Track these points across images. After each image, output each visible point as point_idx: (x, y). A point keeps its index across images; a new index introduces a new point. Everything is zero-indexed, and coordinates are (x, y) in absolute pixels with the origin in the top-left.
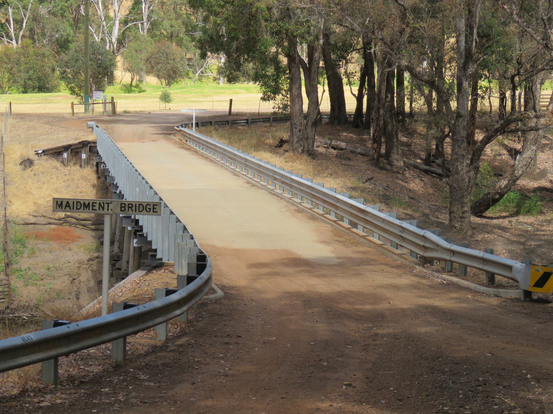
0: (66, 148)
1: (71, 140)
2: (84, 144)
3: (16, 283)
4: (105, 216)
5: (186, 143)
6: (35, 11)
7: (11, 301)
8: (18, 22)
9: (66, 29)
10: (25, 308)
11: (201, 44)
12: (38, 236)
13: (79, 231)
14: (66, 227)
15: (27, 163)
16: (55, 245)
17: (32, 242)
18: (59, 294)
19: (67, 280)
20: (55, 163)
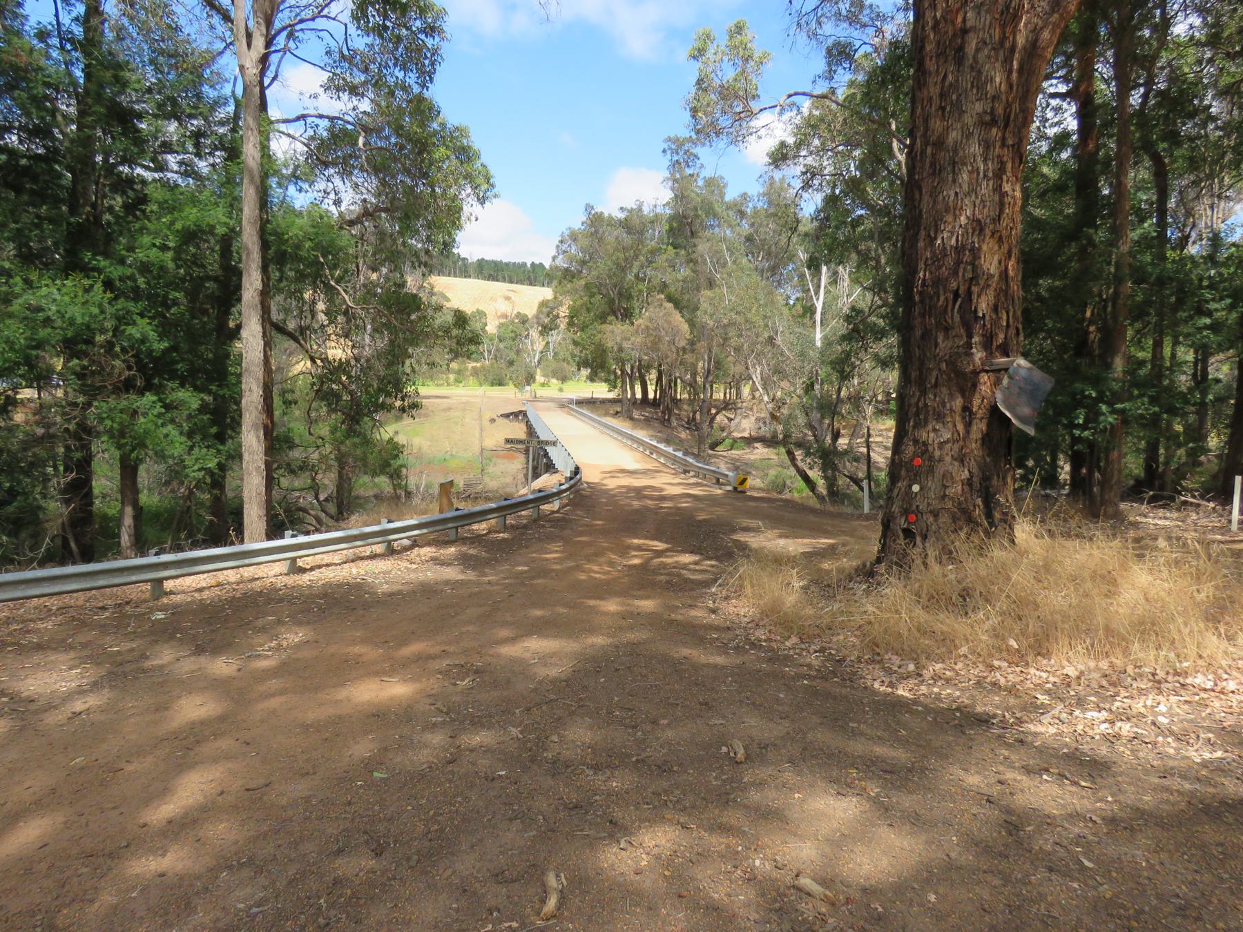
0: (512, 414)
2: (520, 412)
5: (486, 423)
6: (498, 346)
8: (490, 352)
10: (491, 492)
12: (498, 457)
13: (518, 454)
15: (493, 421)
16: (506, 461)
19: (511, 478)
20: (505, 421)
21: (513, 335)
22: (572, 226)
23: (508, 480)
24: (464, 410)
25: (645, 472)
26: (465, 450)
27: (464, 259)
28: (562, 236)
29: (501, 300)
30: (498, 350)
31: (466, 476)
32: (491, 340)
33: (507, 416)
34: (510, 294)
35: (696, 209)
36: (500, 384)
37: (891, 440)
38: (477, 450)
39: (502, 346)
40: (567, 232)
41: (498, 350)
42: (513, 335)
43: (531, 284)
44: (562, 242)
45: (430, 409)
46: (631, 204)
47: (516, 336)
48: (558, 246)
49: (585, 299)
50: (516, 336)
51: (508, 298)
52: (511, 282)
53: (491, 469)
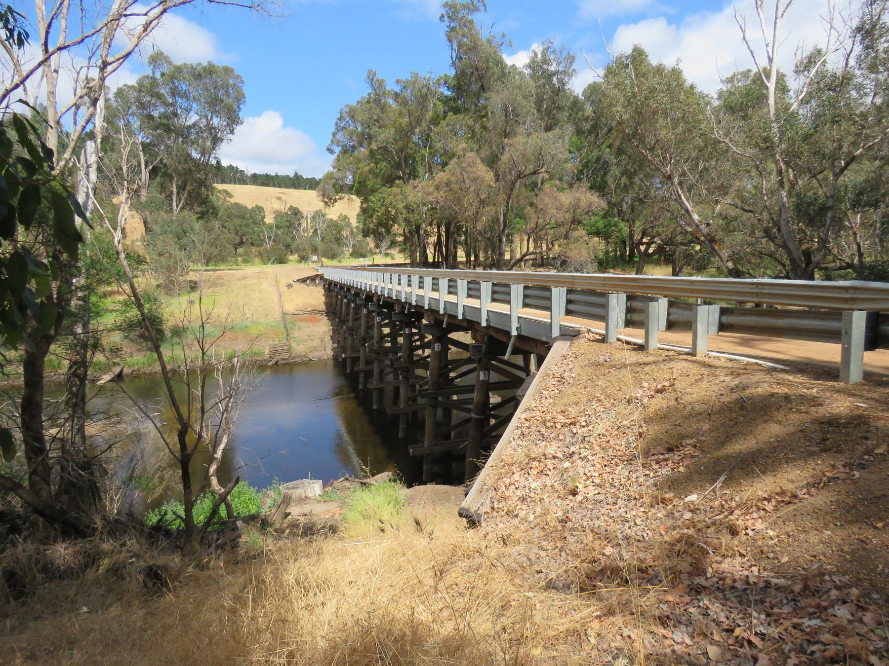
0: (308, 278)
1: (312, 273)
2: (317, 276)
3: (293, 344)
4: (604, 324)
5: (283, 289)
6: (276, 233)
7: (291, 354)
8: (269, 238)
9: (289, 240)
10: (299, 357)
11: (595, 112)
12: (301, 320)
13: (319, 317)
14: (313, 315)
15: (290, 286)
16: (310, 324)
17: (298, 323)
18: (315, 349)
19: (319, 341)
20: (303, 285)
21: (288, 224)
22: (350, 103)
23: (316, 343)
24: (259, 278)
25: (689, 297)
26: (266, 316)
27: (242, 171)
28: (341, 113)
29: (274, 200)
30: (276, 235)
31: (271, 342)
32: (270, 228)
33: (303, 281)
34: (281, 195)
35: (487, 61)
36: (281, 263)
37: (23, 379)
38: (278, 315)
39: (279, 232)
40: (346, 109)
41: (276, 235)
42: (288, 224)
43: (296, 188)
44: (340, 119)
45: (226, 278)
46: (406, 76)
47: (291, 225)
48: (337, 124)
49: (372, 165)
50: (291, 225)
51: (279, 199)
52: (280, 186)
53: (296, 334)
